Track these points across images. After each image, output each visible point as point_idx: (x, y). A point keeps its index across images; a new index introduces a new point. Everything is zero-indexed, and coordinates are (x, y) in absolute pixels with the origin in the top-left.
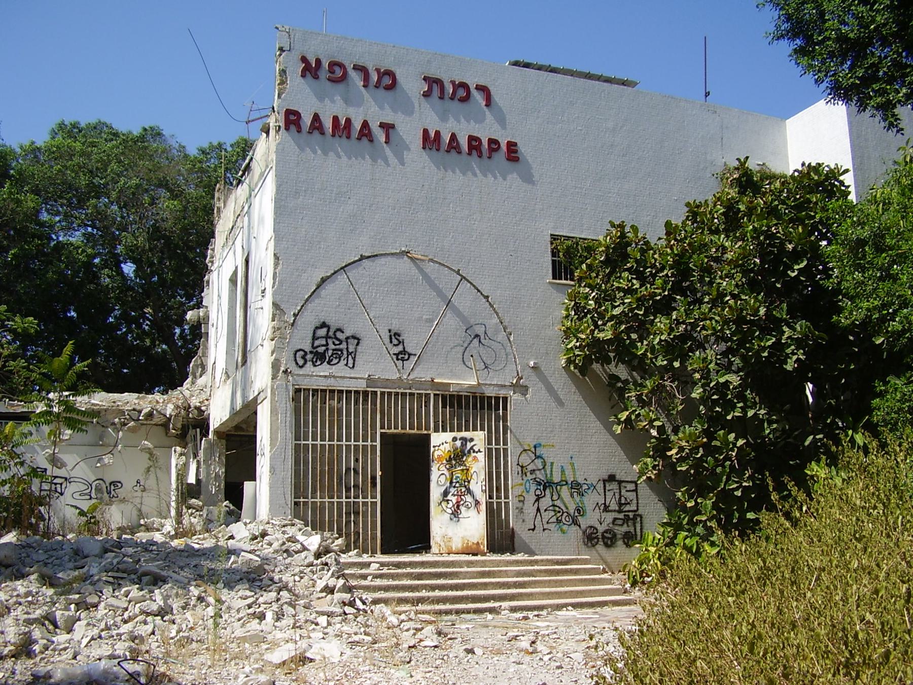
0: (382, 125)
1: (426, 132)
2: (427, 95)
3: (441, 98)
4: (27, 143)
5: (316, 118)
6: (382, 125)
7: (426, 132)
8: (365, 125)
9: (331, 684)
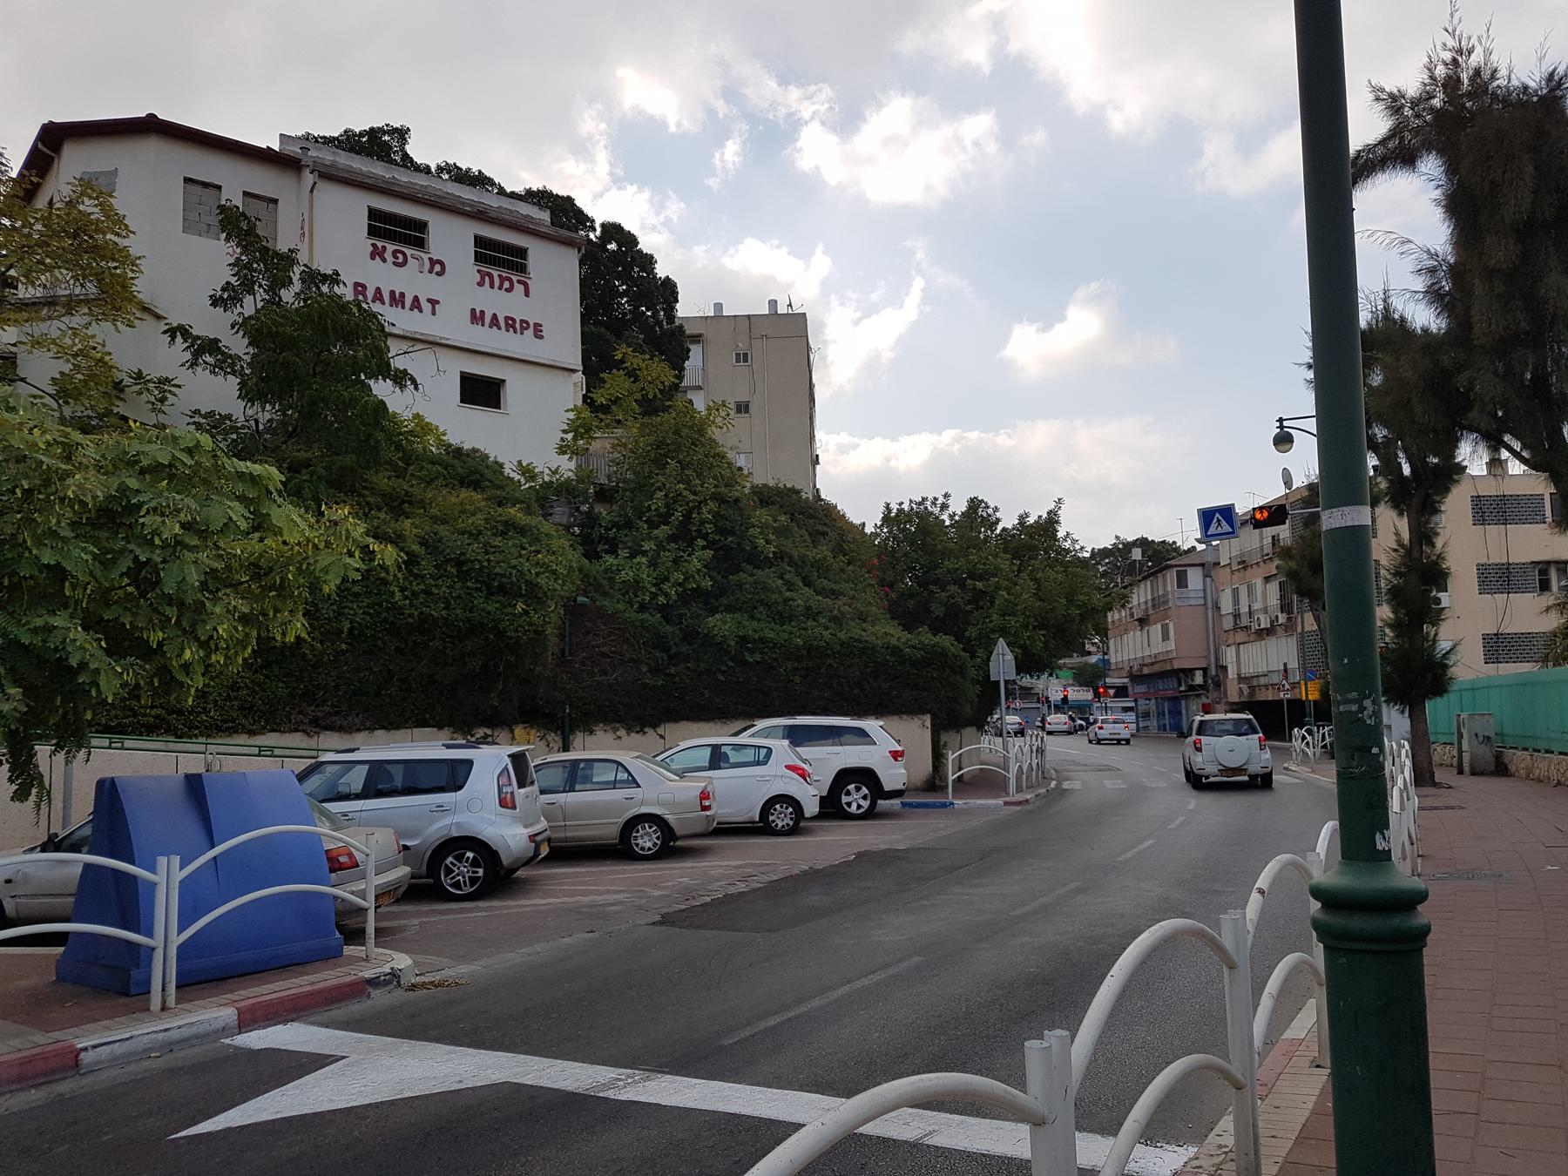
0: (429, 300)
1: (473, 311)
2: (481, 284)
3: (492, 286)
4: (500, 460)
5: (378, 290)
6: (429, 300)
7: (473, 311)
8: (416, 299)
9: (1564, 287)
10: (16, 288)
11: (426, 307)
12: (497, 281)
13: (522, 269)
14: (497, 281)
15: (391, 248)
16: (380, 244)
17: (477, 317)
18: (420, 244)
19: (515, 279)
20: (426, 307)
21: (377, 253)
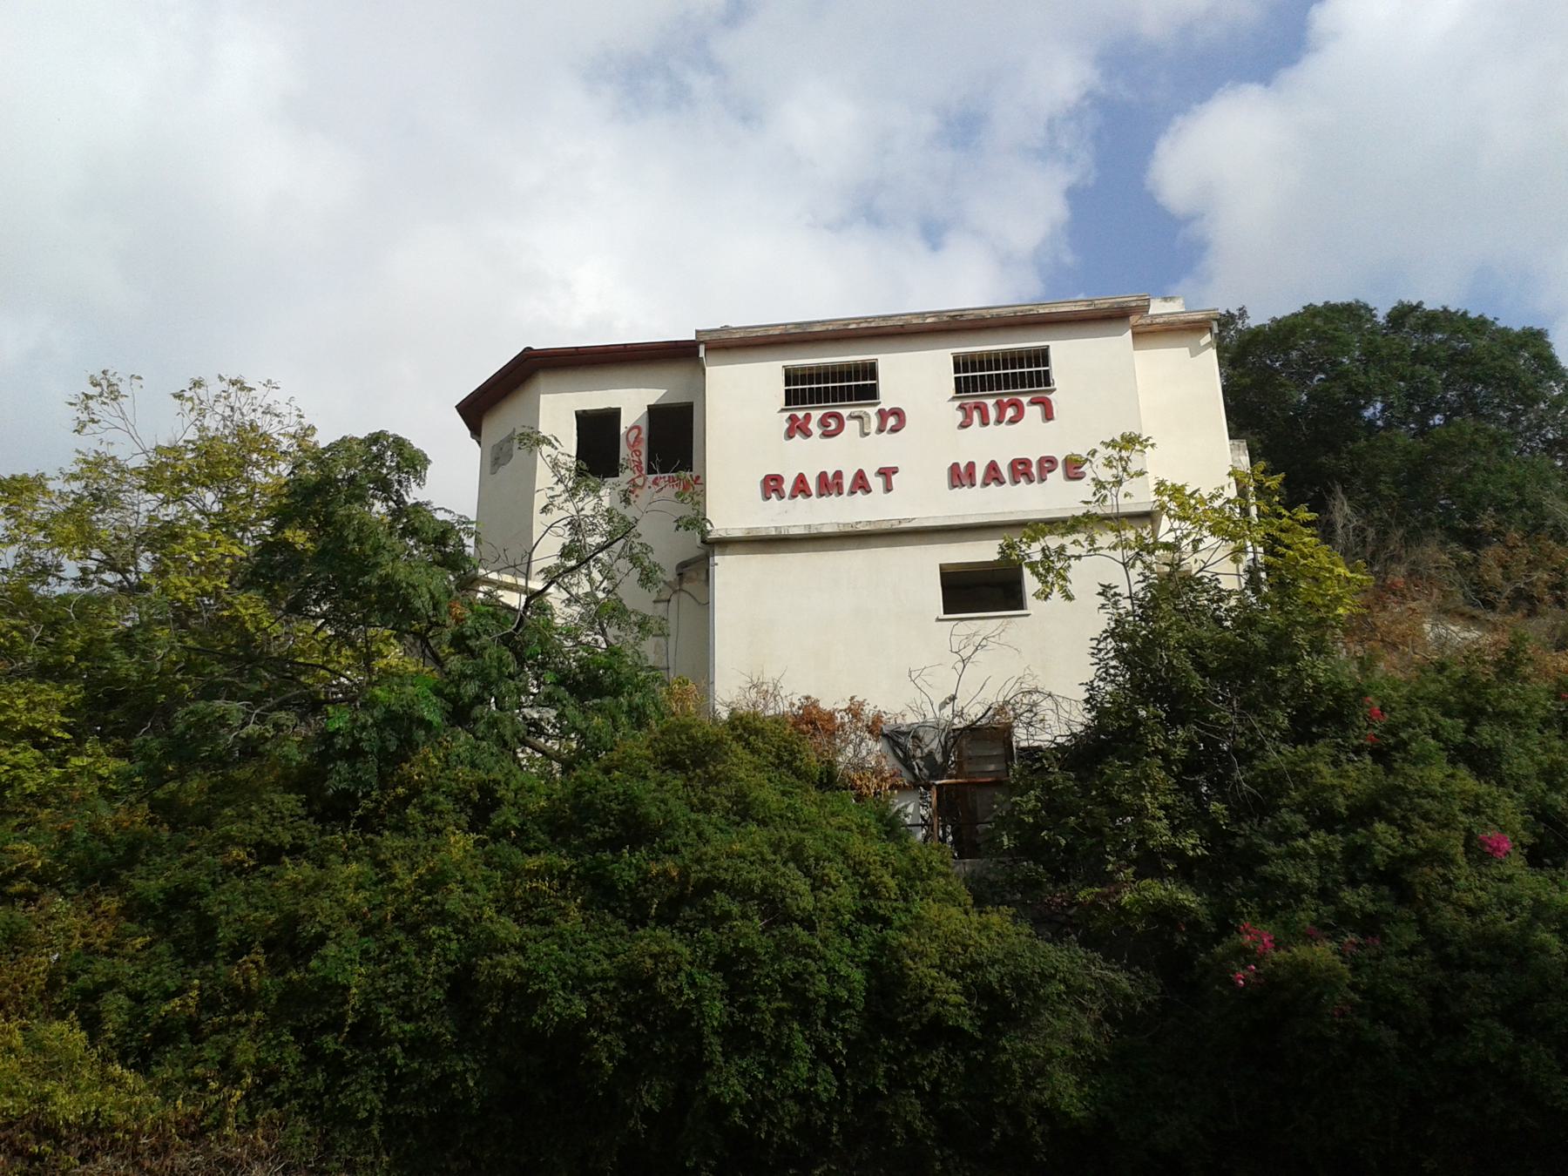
2: (963, 426)
3: (985, 422)
8: (860, 475)
10: (931, 753)
11: (876, 483)
12: (993, 413)
13: (1045, 379)
14: (993, 413)
15: (816, 415)
16: (800, 414)
17: (960, 476)
18: (870, 393)
19: (845, 412)
20: (876, 483)
21: (797, 428)
